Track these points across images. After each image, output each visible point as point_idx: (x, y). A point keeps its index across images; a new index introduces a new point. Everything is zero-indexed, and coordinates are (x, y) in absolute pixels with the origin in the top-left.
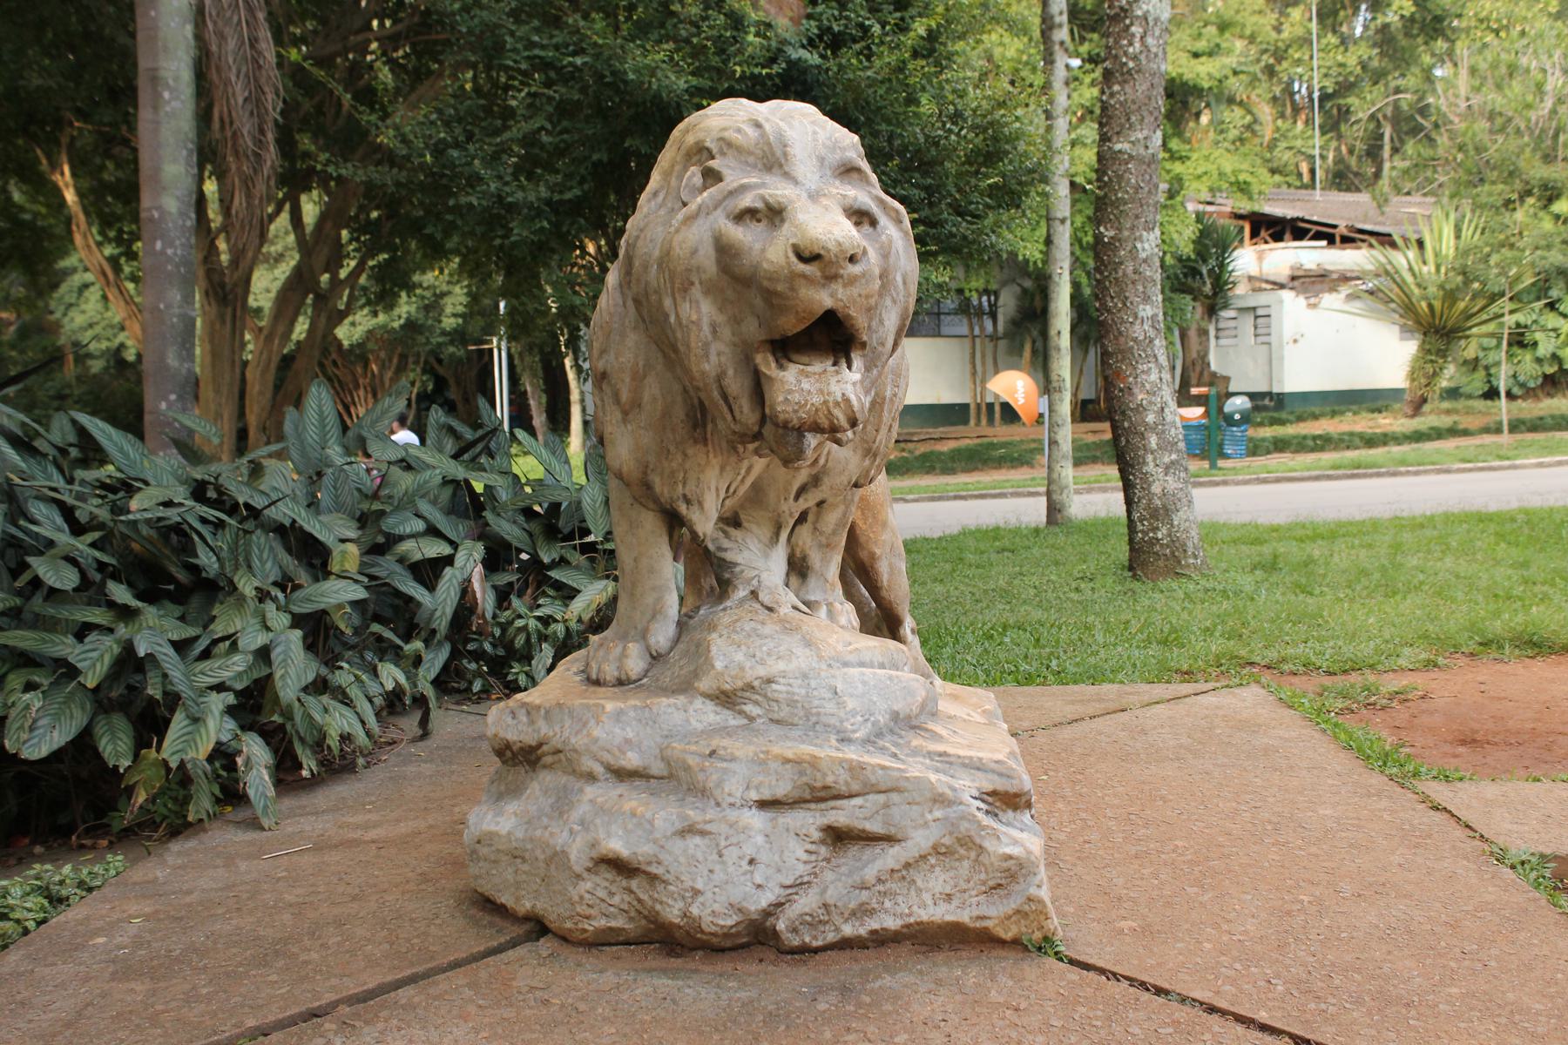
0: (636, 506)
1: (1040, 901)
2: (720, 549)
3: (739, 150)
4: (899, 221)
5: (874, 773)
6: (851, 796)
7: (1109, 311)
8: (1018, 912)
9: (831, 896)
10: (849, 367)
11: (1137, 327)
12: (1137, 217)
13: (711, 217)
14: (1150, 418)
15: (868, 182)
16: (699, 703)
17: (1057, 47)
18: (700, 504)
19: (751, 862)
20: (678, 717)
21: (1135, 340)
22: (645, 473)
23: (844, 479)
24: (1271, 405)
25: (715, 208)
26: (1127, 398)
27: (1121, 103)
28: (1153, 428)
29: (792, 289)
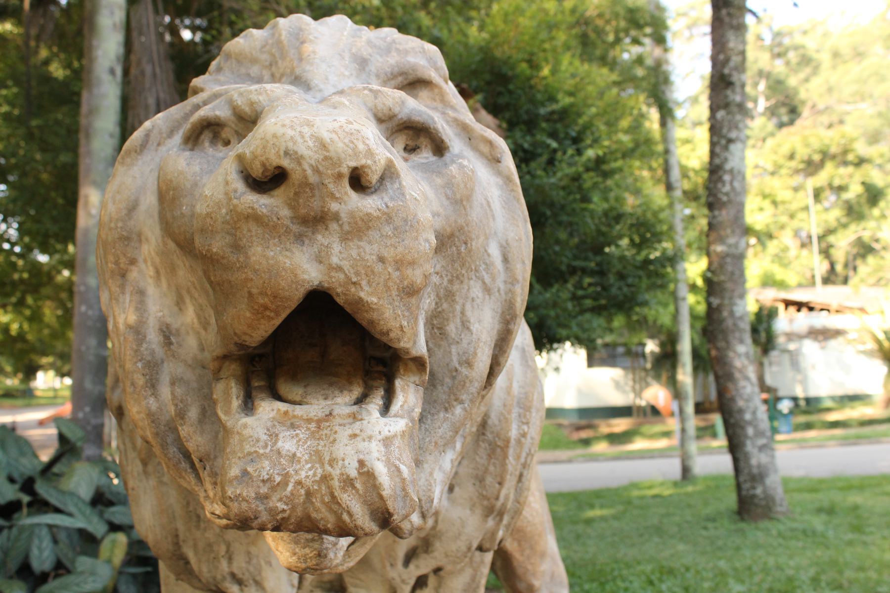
4: (494, 160)
10: (386, 409)
13: (163, 149)
14: (748, 416)
23: (462, 545)
24: (811, 405)
29: (237, 247)
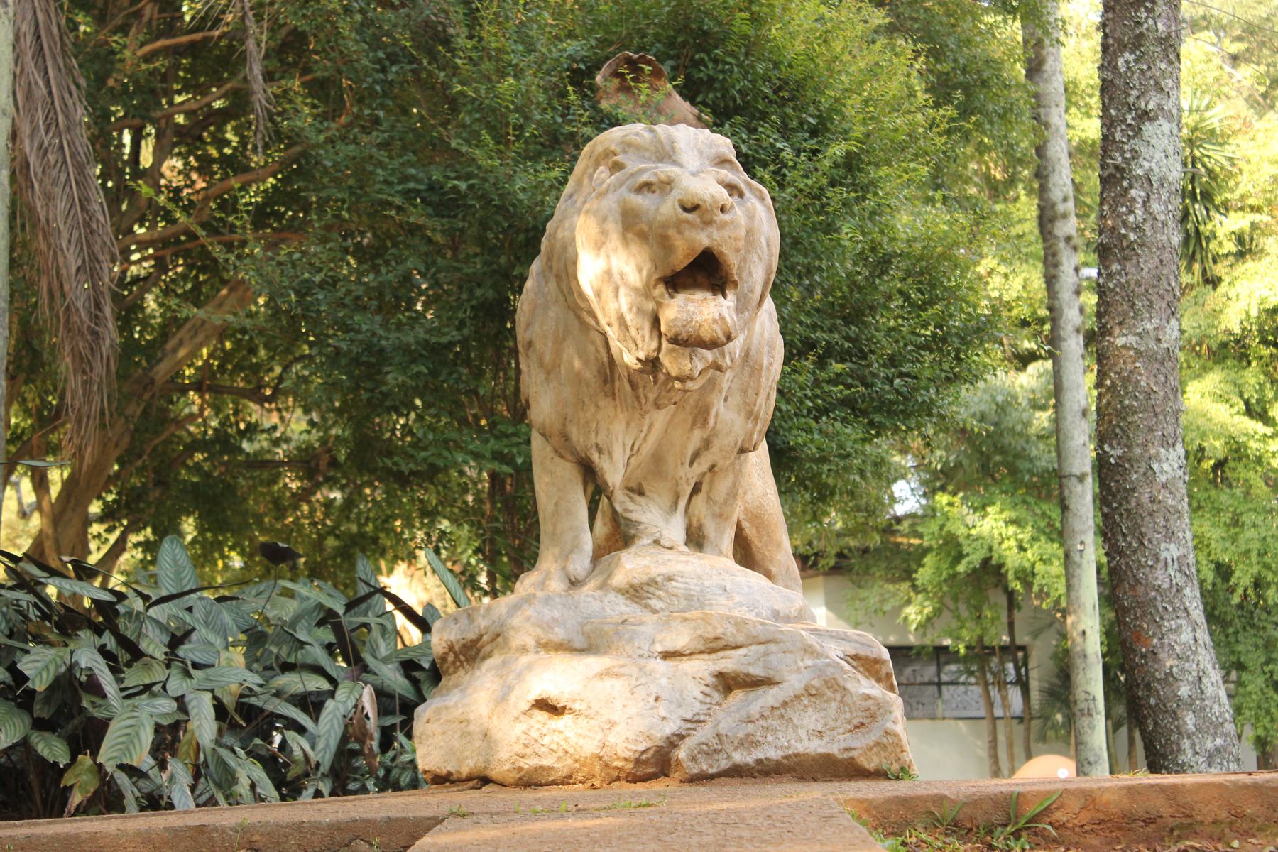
0: (557, 459)
1: (896, 735)
2: (626, 510)
3: (638, 147)
4: (762, 199)
5: (754, 627)
6: (737, 647)
7: (1121, 553)
8: (878, 744)
9: (723, 728)
11: (1159, 572)
12: (1151, 430)
14: (1184, 691)
15: (737, 170)
16: (612, 596)
17: (1062, 245)
18: (610, 453)
19: (657, 699)
20: (595, 606)
21: (1158, 589)
22: (564, 425)
23: (731, 440)
25: (621, 186)
26: (1152, 666)
27: (1122, 286)
28: (1190, 705)
